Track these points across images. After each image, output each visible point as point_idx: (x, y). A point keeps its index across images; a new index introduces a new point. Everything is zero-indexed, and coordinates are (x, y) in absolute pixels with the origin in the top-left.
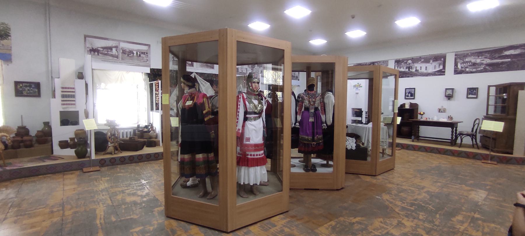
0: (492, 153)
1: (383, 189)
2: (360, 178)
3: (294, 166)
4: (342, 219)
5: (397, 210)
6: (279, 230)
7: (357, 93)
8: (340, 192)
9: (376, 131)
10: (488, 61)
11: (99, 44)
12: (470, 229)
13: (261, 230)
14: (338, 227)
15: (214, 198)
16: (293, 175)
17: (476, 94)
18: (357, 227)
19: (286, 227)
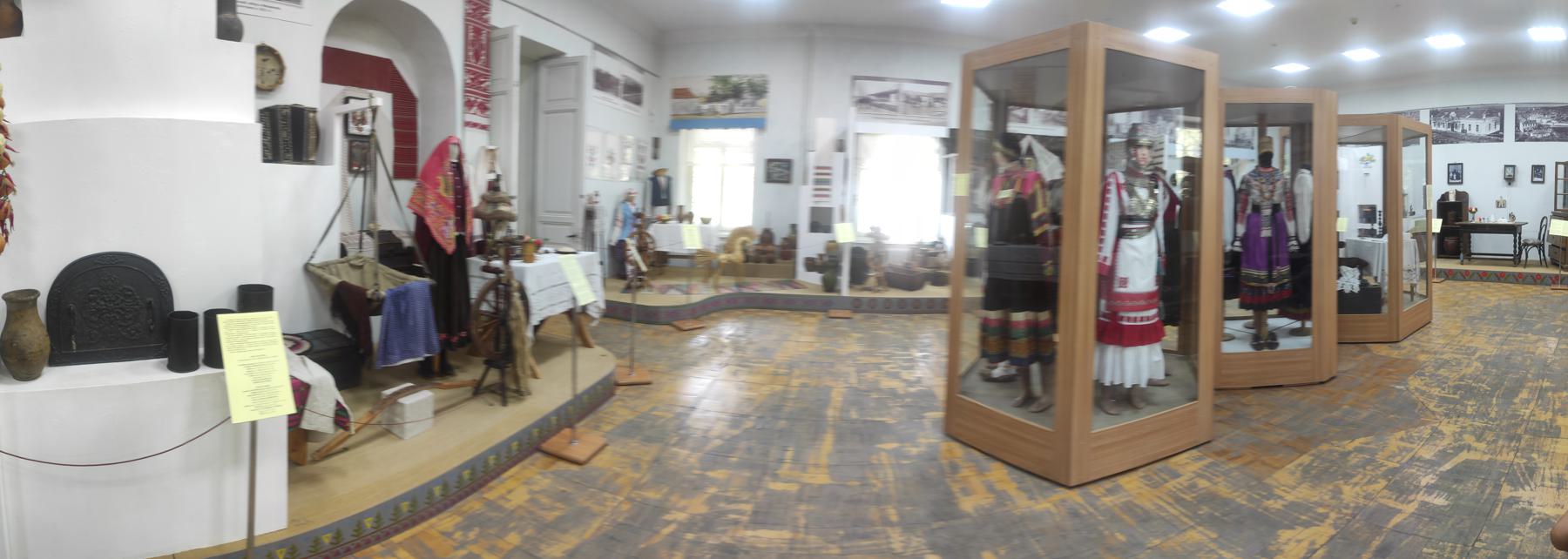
0: (1563, 273)
1: (1409, 367)
2: (1368, 350)
3: (1231, 338)
4: (1325, 447)
5: (1431, 406)
6: (1186, 484)
7: (1367, 174)
8: (1327, 387)
9: (1395, 249)
10: (1555, 124)
11: (872, 88)
12: (1537, 412)
13: (1147, 485)
14: (1317, 467)
15: (1044, 410)
16: (1221, 360)
17: (1543, 176)
18: (1354, 460)
19: (1202, 476)
